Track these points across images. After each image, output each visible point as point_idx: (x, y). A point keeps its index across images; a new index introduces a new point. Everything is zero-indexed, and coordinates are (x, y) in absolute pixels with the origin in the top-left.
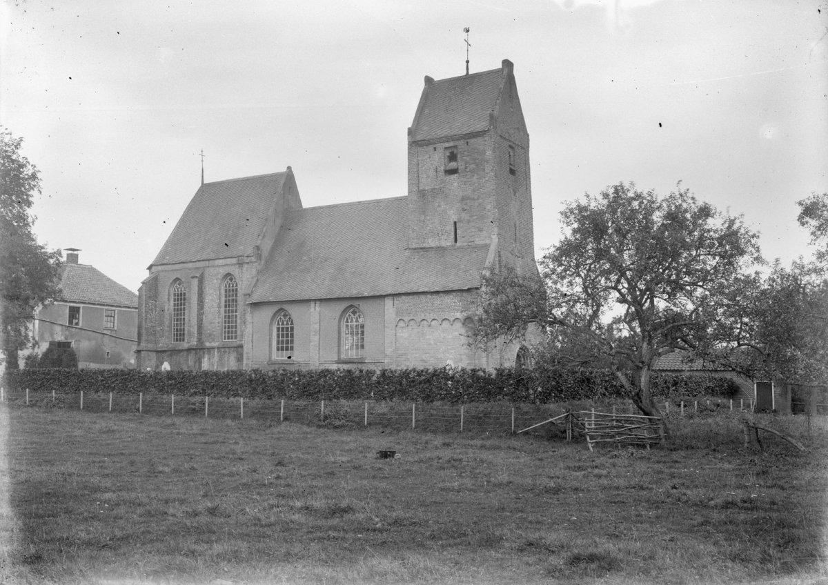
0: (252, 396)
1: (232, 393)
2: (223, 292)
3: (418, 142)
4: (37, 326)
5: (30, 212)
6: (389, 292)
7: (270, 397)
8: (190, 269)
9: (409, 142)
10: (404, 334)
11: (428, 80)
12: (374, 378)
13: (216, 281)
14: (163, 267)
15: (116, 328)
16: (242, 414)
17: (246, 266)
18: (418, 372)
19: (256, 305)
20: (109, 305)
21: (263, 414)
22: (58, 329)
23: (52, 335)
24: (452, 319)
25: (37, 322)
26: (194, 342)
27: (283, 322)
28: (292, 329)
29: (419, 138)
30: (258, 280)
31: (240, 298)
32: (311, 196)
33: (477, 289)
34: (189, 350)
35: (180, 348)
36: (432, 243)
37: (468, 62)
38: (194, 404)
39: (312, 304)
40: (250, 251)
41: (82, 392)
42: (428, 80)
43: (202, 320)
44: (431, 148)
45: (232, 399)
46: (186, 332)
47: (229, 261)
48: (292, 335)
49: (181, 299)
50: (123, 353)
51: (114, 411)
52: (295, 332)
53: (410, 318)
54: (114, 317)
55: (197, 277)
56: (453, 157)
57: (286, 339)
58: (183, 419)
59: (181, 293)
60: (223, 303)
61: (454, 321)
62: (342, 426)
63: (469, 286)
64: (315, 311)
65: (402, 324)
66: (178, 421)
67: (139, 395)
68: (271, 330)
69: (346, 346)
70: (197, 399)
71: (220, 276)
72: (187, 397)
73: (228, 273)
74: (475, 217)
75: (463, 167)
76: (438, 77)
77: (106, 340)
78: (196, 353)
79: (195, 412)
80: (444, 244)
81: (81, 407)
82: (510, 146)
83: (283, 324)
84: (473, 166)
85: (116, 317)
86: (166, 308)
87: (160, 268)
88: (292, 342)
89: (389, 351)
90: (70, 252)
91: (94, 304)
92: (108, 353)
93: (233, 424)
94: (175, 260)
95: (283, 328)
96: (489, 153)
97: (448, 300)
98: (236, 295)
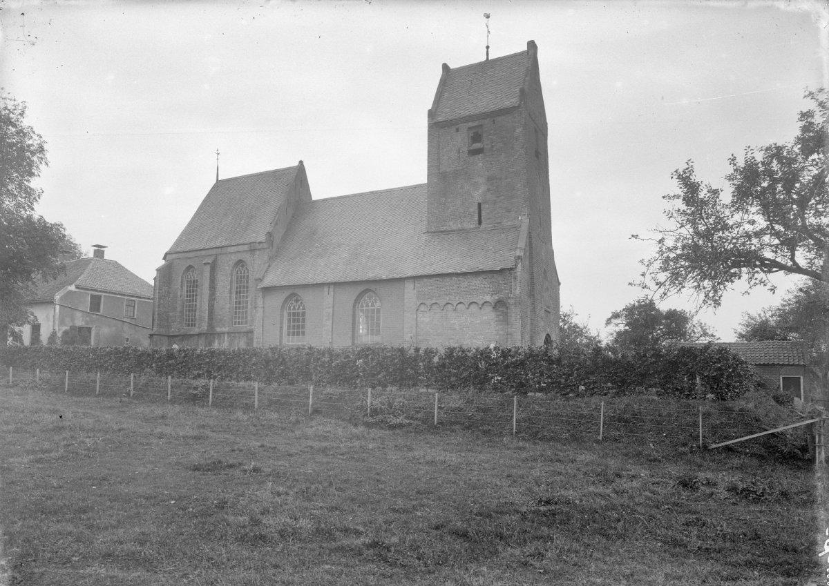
0: (268, 381)
1: (243, 376)
2: (234, 278)
3: (438, 125)
4: (57, 311)
5: (34, 183)
6: (410, 275)
7: (291, 383)
8: (203, 257)
9: (429, 124)
10: (425, 318)
11: (445, 67)
12: (436, 359)
13: (227, 268)
14: (177, 255)
15: (135, 317)
16: (256, 403)
17: (258, 252)
18: (503, 351)
19: (267, 290)
20: (130, 296)
21: (285, 403)
22: (78, 314)
23: (73, 320)
24: (481, 303)
25: (58, 307)
26: (205, 327)
28: (304, 314)
29: (440, 119)
30: (269, 266)
31: (250, 284)
32: (319, 190)
33: (511, 269)
34: (199, 335)
35: (192, 333)
36: (452, 225)
37: (488, 47)
38: (195, 388)
39: (326, 289)
40: (262, 238)
42: (445, 67)
43: (213, 306)
44: (454, 129)
45: (242, 383)
46: (197, 317)
47: (241, 248)
48: (304, 320)
49: (194, 285)
50: (142, 339)
51: (102, 394)
52: (307, 316)
53: (434, 301)
54: (134, 307)
55: (209, 263)
56: (477, 138)
57: (297, 324)
58: (178, 408)
59: (194, 281)
60: (234, 290)
62: (401, 426)
63: (502, 267)
64: (328, 297)
65: (423, 308)
66: (172, 410)
67: (66, 373)
68: (282, 316)
69: (362, 329)
70: (202, 382)
71: (232, 263)
72: (187, 379)
73: (240, 260)
75: (490, 146)
76: (453, 65)
77: (126, 327)
78: (206, 338)
79: (197, 399)
80: (467, 226)
81: (66, 389)
83: (294, 309)
84: (501, 145)
85: (136, 307)
86: (179, 294)
87: (174, 256)
88: (303, 327)
89: (407, 337)
90: (96, 248)
91: (115, 294)
92: (128, 339)
93: (245, 417)
94: (189, 248)
95: (294, 314)
96: (519, 130)
97: (476, 282)
98: (247, 282)
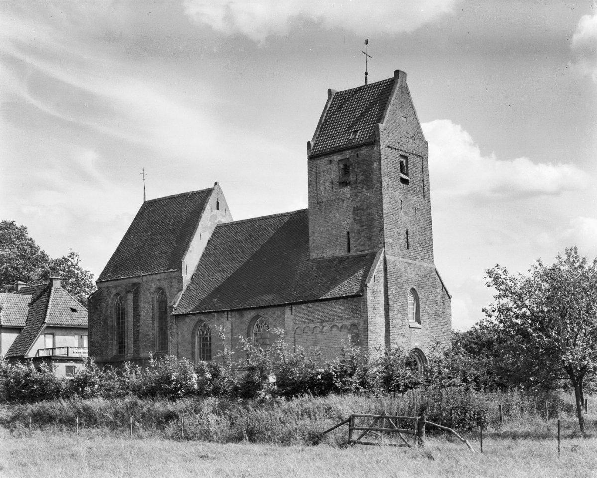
11: (330, 91)
24: (340, 325)
27: (203, 333)
37: (366, 73)
41: (131, 422)
49: (121, 314)
61: (341, 327)
74: (365, 227)
82: (402, 156)
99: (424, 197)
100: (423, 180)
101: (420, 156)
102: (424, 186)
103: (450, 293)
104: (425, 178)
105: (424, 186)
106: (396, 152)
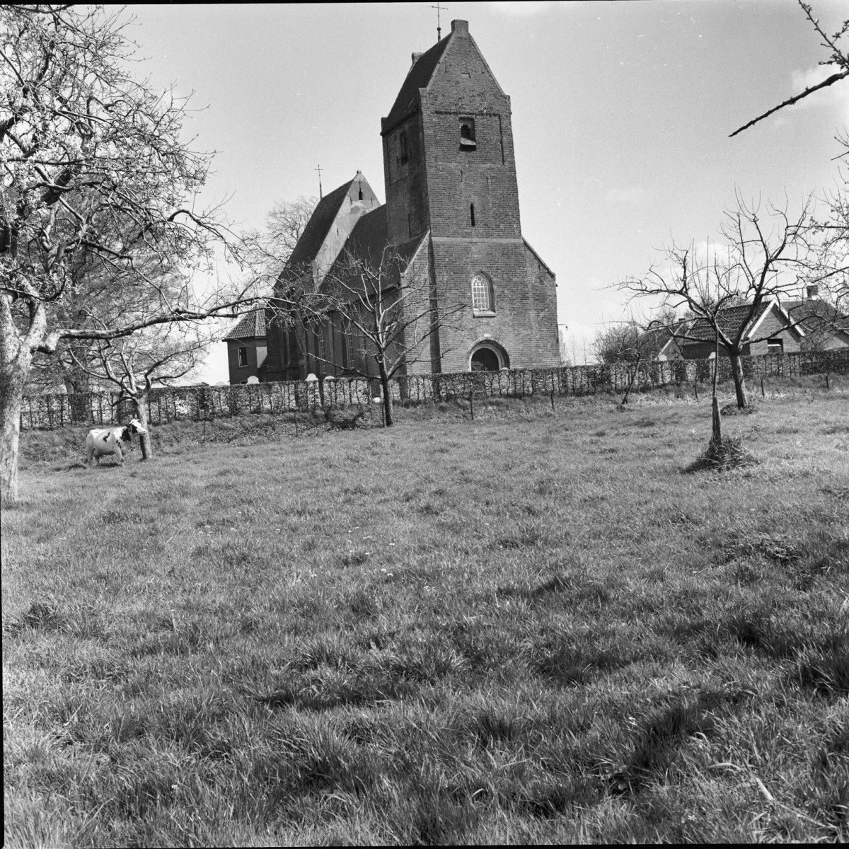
37: (439, 29)
99: (503, 162)
100: (501, 142)
101: (495, 115)
102: (502, 149)
103: (553, 270)
104: (505, 139)
105: (502, 149)
106: (451, 118)
